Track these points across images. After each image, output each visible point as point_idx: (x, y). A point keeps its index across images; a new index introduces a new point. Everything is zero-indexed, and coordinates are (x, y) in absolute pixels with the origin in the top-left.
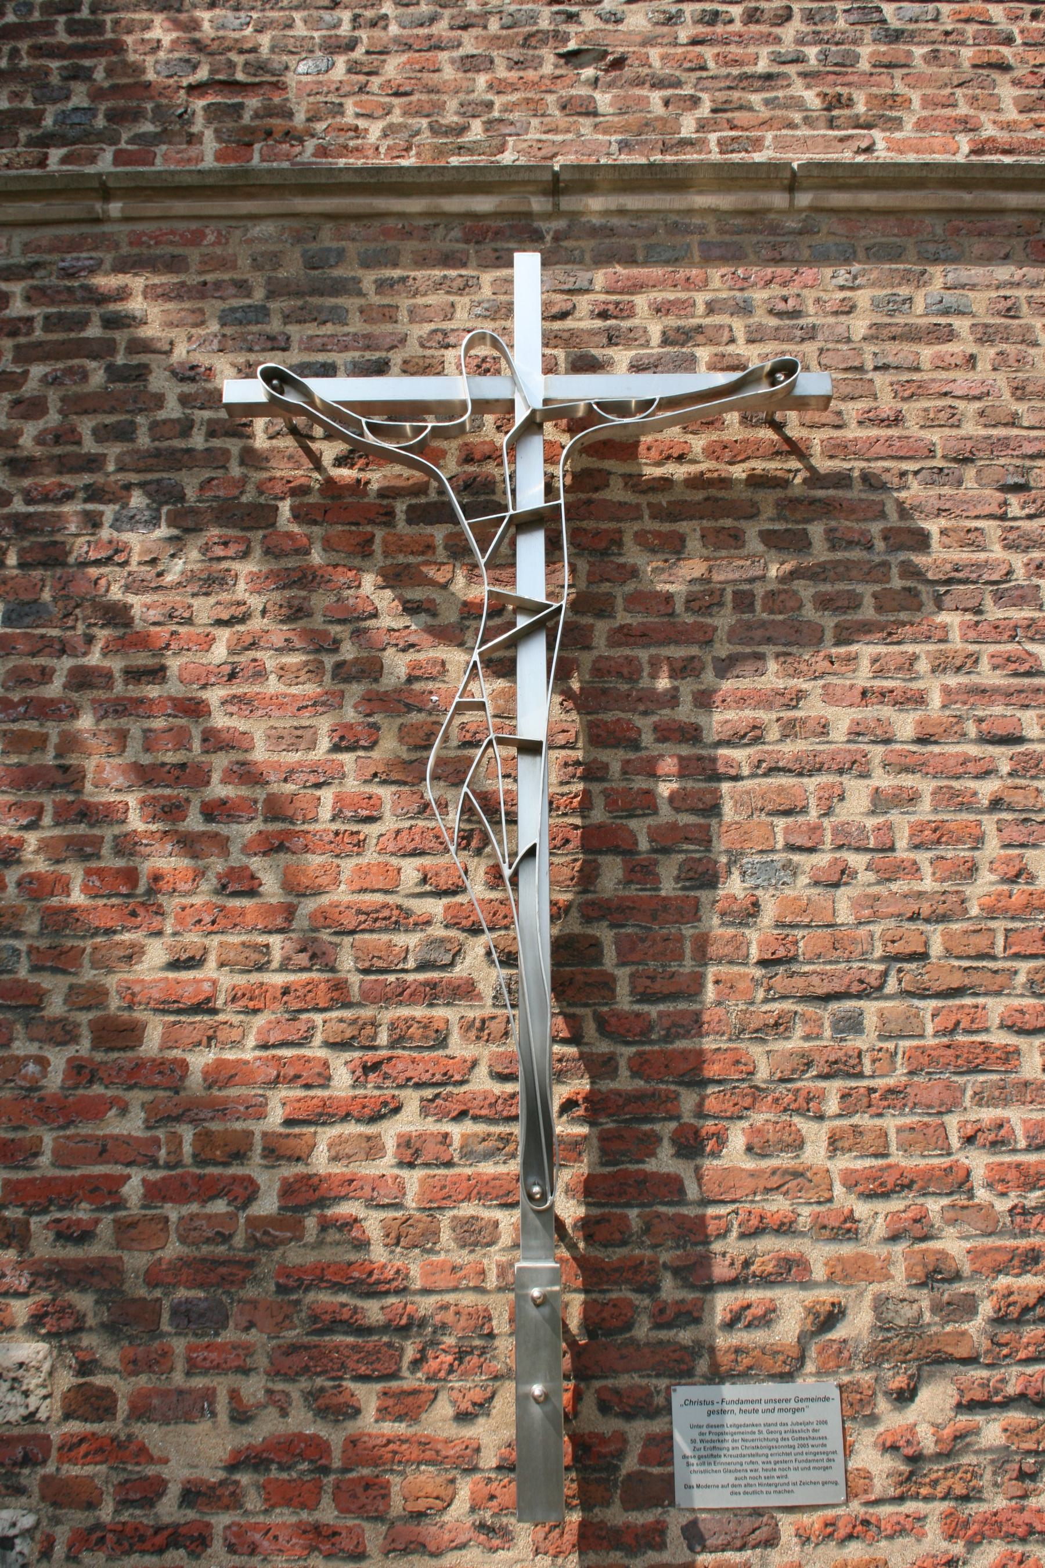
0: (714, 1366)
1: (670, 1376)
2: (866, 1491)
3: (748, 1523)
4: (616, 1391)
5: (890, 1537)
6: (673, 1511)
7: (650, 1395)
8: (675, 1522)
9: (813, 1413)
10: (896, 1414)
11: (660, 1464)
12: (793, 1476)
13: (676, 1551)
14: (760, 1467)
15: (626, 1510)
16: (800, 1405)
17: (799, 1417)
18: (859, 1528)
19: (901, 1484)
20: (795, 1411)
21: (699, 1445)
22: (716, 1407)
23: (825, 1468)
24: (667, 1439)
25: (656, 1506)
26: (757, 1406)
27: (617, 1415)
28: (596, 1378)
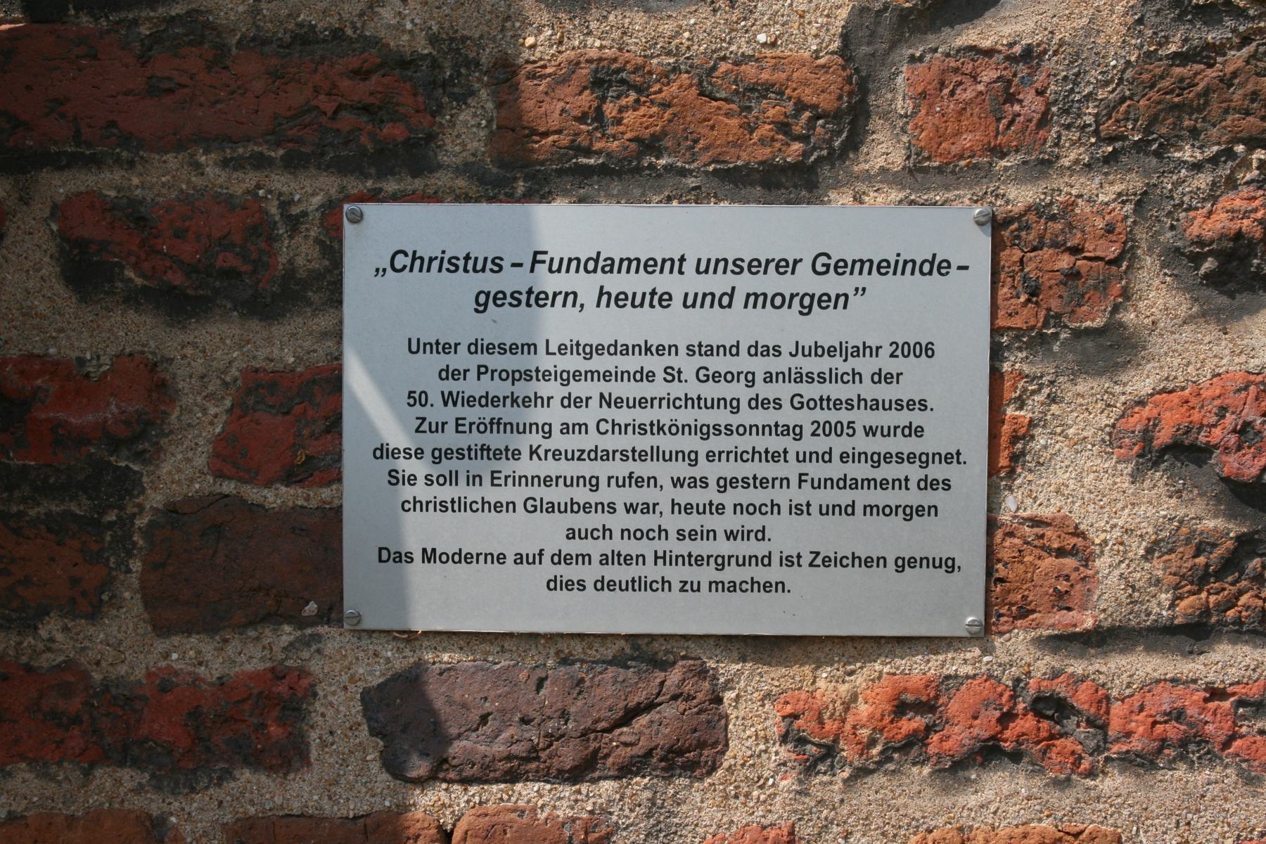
0: (513, 133)
1: (342, 167)
2: (1061, 600)
3: (610, 688)
4: (134, 215)
5: (1140, 764)
6: (334, 639)
7: (261, 230)
8: (342, 678)
9: (880, 313)
10: (1209, 332)
11: (290, 478)
12: (786, 534)
13: (337, 776)
14: (664, 496)
15: (162, 629)
16: (832, 284)
17: (826, 327)
18: (1026, 724)
19: (1202, 579)
20: (809, 304)
21: (438, 412)
22: (510, 281)
23: (912, 512)
24: (316, 396)
25: (274, 617)
26: (663, 282)
27: (133, 299)
28: (60, 163)
